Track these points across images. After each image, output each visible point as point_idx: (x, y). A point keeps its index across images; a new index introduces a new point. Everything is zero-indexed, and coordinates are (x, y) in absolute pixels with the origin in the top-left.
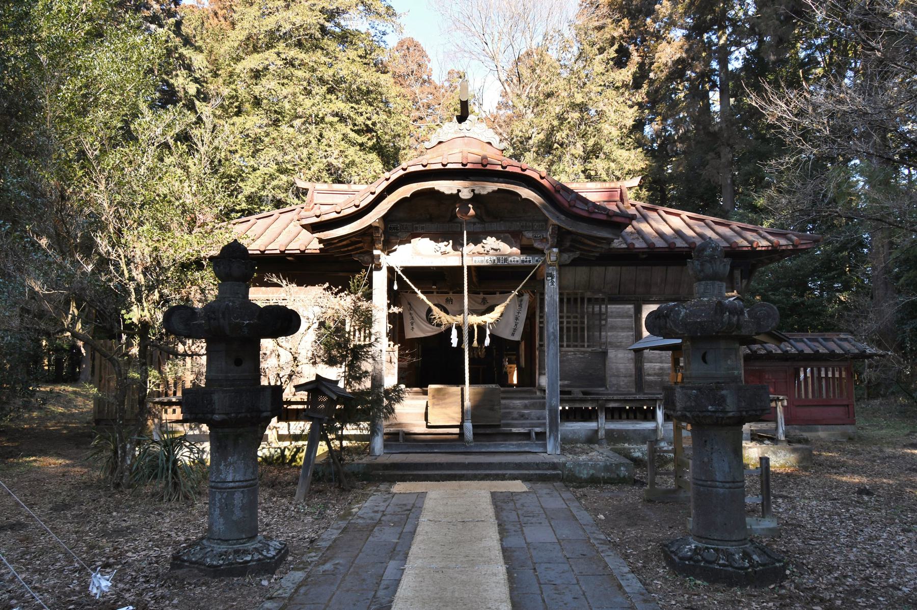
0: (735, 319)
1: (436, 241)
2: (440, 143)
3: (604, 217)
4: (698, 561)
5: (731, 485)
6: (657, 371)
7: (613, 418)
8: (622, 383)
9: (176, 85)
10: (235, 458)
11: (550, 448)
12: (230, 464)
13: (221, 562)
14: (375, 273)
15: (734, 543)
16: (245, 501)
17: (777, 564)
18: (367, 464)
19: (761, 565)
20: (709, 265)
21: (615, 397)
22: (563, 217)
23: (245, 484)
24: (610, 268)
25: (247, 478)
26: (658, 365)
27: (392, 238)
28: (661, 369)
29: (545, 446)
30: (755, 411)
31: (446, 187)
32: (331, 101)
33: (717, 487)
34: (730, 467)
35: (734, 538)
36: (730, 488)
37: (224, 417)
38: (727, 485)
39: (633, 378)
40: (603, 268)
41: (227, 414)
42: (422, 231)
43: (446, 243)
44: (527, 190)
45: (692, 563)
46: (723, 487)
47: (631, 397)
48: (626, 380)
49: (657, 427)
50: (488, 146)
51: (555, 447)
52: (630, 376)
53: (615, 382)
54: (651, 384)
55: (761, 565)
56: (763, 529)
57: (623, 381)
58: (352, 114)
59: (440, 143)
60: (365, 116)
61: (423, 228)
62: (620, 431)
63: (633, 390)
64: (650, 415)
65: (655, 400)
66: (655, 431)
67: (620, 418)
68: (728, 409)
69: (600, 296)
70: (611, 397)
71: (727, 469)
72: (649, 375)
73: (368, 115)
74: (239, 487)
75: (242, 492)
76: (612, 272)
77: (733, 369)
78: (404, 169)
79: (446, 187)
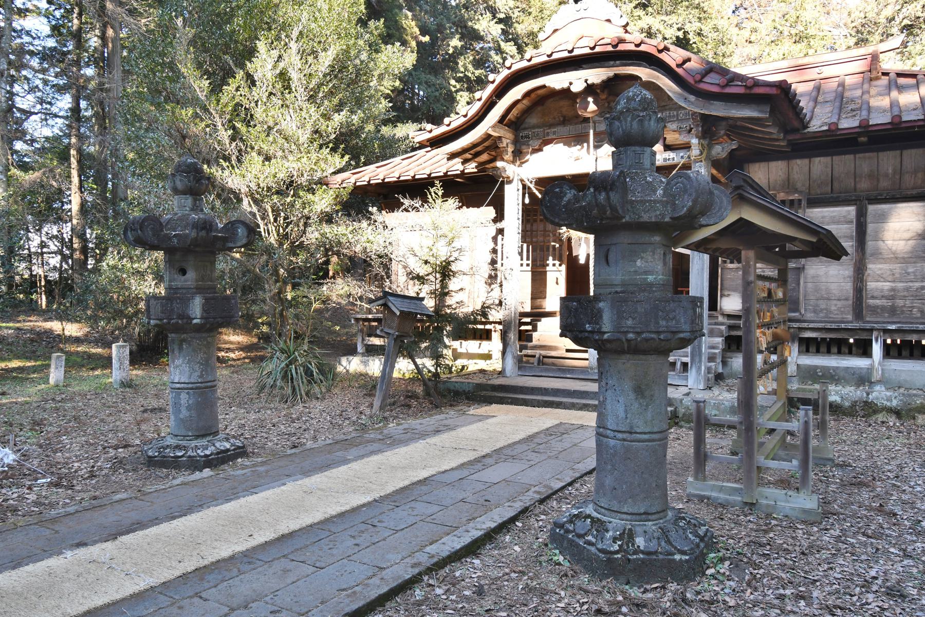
0: (602, 197)
1: (569, 145)
2: (555, 31)
3: (741, 90)
4: (568, 531)
5: (625, 436)
6: (886, 293)
7: (808, 351)
8: (833, 308)
9: (481, 29)
10: (181, 361)
11: (691, 382)
12: (177, 367)
13: (156, 454)
14: (507, 187)
15: (625, 516)
16: (191, 402)
17: (677, 557)
18: (477, 384)
19: (643, 552)
20: (617, 123)
21: (812, 325)
22: (692, 98)
23: (190, 386)
24: (817, 160)
25: (193, 381)
26: (887, 285)
27: (524, 147)
28: (893, 290)
29: (686, 379)
30: (658, 333)
31: (557, 81)
32: (640, 18)
33: (607, 437)
34: (626, 411)
35: (625, 510)
36: (624, 440)
37: (158, 322)
38: (620, 436)
39: (850, 302)
40: (806, 161)
41: (160, 320)
42: (554, 137)
43: (579, 147)
44: (648, 70)
45: (562, 532)
46: (614, 438)
47: (850, 326)
48: (840, 304)
49: (872, 365)
50: (607, 24)
51: (697, 381)
52: (847, 299)
53: (823, 307)
54: (874, 310)
55: (643, 552)
56: (793, 509)
57: (834, 306)
58: (662, 28)
59: (555, 31)
60: (676, 27)
61: (554, 133)
62: (825, 369)
63: (850, 317)
64: (864, 349)
65: (871, 330)
66: (870, 370)
67: (829, 352)
68: (604, 329)
69: (796, 196)
70: (805, 325)
71: (622, 414)
72: (873, 297)
73: (679, 25)
74: (187, 389)
75: (188, 393)
76: (820, 165)
77: (646, 273)
78: (509, 68)
79: (557, 81)
